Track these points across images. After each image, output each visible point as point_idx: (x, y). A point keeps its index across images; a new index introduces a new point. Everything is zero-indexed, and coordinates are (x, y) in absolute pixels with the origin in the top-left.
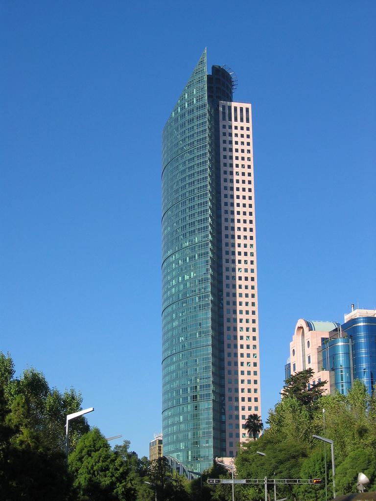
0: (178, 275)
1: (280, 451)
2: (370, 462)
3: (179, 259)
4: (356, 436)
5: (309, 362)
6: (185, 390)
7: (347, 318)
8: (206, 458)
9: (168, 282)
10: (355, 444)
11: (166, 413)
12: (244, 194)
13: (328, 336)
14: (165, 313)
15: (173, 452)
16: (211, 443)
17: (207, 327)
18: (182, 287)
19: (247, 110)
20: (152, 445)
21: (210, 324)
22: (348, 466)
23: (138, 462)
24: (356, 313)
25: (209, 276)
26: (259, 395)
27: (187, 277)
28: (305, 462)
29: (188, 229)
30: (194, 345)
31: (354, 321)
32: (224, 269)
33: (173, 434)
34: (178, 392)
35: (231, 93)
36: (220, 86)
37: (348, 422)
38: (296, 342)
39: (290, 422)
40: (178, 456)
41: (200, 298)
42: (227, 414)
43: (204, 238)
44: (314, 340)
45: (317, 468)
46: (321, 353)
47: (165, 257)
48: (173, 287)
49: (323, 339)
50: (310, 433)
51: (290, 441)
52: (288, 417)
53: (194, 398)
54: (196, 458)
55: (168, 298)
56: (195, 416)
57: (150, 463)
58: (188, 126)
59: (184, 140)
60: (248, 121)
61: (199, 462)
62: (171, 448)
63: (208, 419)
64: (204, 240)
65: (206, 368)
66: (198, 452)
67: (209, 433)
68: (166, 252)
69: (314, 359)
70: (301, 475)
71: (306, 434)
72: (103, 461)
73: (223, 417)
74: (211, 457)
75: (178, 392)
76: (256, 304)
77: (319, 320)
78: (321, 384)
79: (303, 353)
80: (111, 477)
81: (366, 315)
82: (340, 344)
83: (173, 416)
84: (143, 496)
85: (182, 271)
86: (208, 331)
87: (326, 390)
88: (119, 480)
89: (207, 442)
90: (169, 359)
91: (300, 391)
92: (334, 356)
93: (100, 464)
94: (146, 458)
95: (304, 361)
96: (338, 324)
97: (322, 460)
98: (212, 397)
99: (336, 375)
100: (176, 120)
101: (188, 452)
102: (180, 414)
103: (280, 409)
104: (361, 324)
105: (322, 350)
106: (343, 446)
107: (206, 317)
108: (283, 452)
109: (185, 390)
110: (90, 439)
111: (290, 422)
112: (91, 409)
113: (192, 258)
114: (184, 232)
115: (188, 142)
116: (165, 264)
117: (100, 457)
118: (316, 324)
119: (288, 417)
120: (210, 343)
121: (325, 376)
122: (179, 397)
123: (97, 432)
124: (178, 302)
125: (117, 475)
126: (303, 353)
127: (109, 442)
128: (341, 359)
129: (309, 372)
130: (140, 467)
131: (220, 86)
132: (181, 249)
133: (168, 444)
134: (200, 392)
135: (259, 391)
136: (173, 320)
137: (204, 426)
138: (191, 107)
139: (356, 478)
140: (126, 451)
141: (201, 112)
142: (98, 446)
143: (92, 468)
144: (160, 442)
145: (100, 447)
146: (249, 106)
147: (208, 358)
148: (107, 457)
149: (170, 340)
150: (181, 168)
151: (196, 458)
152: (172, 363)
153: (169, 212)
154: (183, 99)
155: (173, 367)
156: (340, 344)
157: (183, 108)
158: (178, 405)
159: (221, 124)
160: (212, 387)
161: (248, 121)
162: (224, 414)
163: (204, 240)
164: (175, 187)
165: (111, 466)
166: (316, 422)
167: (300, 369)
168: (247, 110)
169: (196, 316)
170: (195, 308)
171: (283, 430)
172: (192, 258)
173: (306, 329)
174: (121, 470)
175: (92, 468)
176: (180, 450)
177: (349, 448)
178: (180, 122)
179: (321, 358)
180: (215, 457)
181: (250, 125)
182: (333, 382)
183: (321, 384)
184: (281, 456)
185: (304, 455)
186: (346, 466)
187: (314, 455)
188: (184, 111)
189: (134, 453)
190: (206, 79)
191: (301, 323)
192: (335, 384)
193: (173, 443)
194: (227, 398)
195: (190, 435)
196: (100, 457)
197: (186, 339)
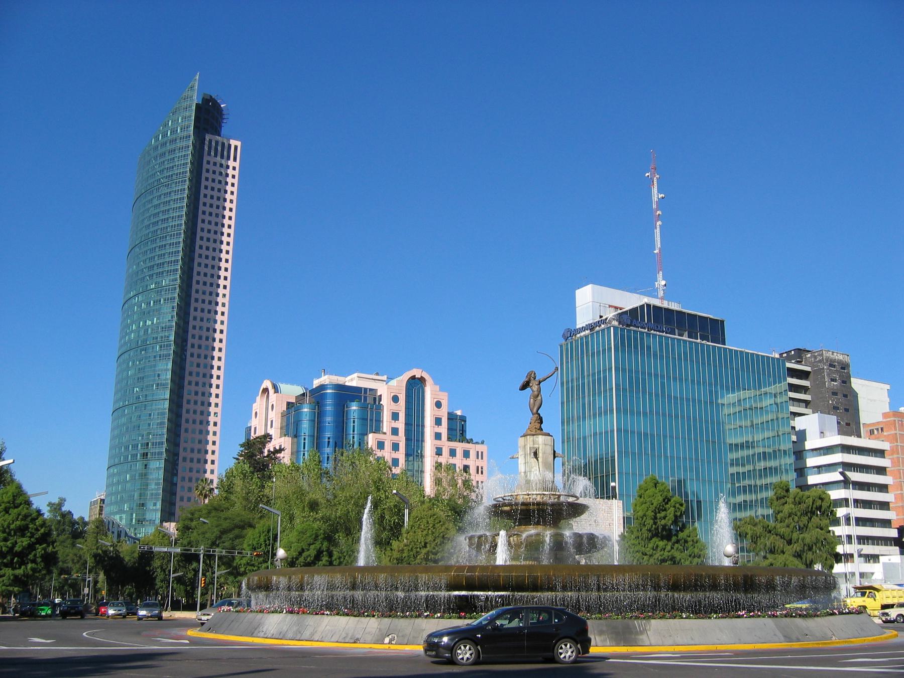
0: (140, 319)
1: (226, 519)
2: (317, 536)
3: (142, 301)
4: (306, 509)
5: (272, 426)
6: (135, 446)
7: (316, 383)
8: (152, 522)
9: (128, 326)
10: (304, 517)
11: (111, 470)
12: (210, 227)
13: (294, 401)
14: (121, 360)
15: (117, 513)
16: (159, 506)
17: (166, 379)
18: (142, 333)
19: (236, 147)
20: (93, 504)
21: (169, 376)
22: (294, 540)
23: (73, 523)
24: (325, 379)
25: (174, 324)
26: (220, 460)
27: (149, 323)
28: (249, 532)
29: (156, 270)
30: (149, 398)
31: (322, 387)
32: (191, 318)
33: (117, 493)
34: (127, 448)
35: (221, 127)
36: (209, 117)
37: (300, 493)
38: (259, 405)
39: (239, 489)
40: (121, 518)
41: (161, 347)
42: (180, 475)
43: (172, 281)
44: (278, 403)
45: (262, 540)
46: (285, 418)
47: (127, 297)
48: (132, 331)
49: (288, 404)
50: (257, 503)
51: (238, 509)
52: (238, 483)
53: (145, 455)
54: (140, 521)
55: (125, 343)
56: (144, 476)
57: (86, 524)
58: (168, 157)
59: (162, 171)
60: (235, 160)
61: (143, 526)
62: (114, 508)
63: (159, 479)
64: (172, 283)
65: (162, 423)
66: (144, 514)
67: (157, 494)
68: (129, 292)
69: (277, 424)
70: (245, 546)
71: (257, 503)
72: (22, 520)
73: (175, 479)
74: (158, 521)
75: (127, 448)
76: (223, 359)
77: (287, 383)
78: (281, 450)
79: (266, 417)
80: (31, 537)
81: (335, 382)
82: (306, 409)
83: (119, 474)
84: (73, 560)
85: (145, 315)
86: (167, 384)
87: (286, 458)
88: (40, 541)
89: (155, 504)
90: (120, 411)
91: (255, 456)
92: (297, 423)
93: (18, 523)
94: (83, 518)
95: (266, 425)
96: (306, 389)
97: (268, 532)
98: (164, 455)
99: (298, 444)
100: (156, 148)
101: (132, 515)
102: (127, 472)
103: (230, 475)
104: (329, 391)
105: (285, 415)
106: (292, 518)
107: (166, 369)
108: (228, 521)
109: (135, 446)
110: (10, 494)
111: (239, 489)
112: (11, 461)
113: (157, 302)
114: (151, 273)
115: (166, 174)
116: (126, 306)
117: (19, 515)
118: (283, 387)
119: (238, 483)
120: (168, 396)
121: (286, 442)
122: (127, 454)
123: (19, 487)
124: (136, 349)
125: (37, 536)
126: (266, 417)
127: (31, 499)
128: (305, 426)
129: (267, 437)
130: (75, 530)
131: (209, 117)
132: (146, 290)
133: (111, 504)
134: (151, 449)
135: (217, 453)
136: (128, 368)
137: (153, 486)
138: (174, 136)
139: (113, 616)
140: (60, 509)
141: (184, 144)
142: (18, 501)
143: (8, 527)
144: (103, 501)
145: (21, 504)
146: (239, 144)
147: (164, 414)
148: (26, 517)
149: (123, 389)
150: (156, 202)
151: (140, 521)
152: (123, 415)
153: (137, 250)
154: (166, 125)
155: (124, 420)
156: (306, 409)
157: (165, 135)
158: (126, 461)
159: (206, 158)
160: (165, 445)
161: (235, 160)
162: (176, 475)
163: (172, 283)
164: (146, 223)
165: (31, 526)
166: (267, 491)
167: (260, 432)
168: (236, 147)
169: (155, 366)
170: (155, 357)
171: (233, 497)
172: (157, 302)
173: (271, 391)
174: (42, 530)
175: (8, 527)
176: (124, 512)
177: (298, 521)
178: (160, 151)
179: (285, 424)
180: (161, 522)
181: (237, 164)
182: (295, 450)
183: (281, 450)
184: (226, 525)
185: (251, 526)
186: (291, 539)
187: (261, 526)
188: (165, 139)
189: (70, 512)
190: (194, 108)
191: (267, 384)
192: (295, 453)
193: (116, 503)
194: (181, 458)
195: (136, 496)
196: (19, 515)
197: (142, 390)
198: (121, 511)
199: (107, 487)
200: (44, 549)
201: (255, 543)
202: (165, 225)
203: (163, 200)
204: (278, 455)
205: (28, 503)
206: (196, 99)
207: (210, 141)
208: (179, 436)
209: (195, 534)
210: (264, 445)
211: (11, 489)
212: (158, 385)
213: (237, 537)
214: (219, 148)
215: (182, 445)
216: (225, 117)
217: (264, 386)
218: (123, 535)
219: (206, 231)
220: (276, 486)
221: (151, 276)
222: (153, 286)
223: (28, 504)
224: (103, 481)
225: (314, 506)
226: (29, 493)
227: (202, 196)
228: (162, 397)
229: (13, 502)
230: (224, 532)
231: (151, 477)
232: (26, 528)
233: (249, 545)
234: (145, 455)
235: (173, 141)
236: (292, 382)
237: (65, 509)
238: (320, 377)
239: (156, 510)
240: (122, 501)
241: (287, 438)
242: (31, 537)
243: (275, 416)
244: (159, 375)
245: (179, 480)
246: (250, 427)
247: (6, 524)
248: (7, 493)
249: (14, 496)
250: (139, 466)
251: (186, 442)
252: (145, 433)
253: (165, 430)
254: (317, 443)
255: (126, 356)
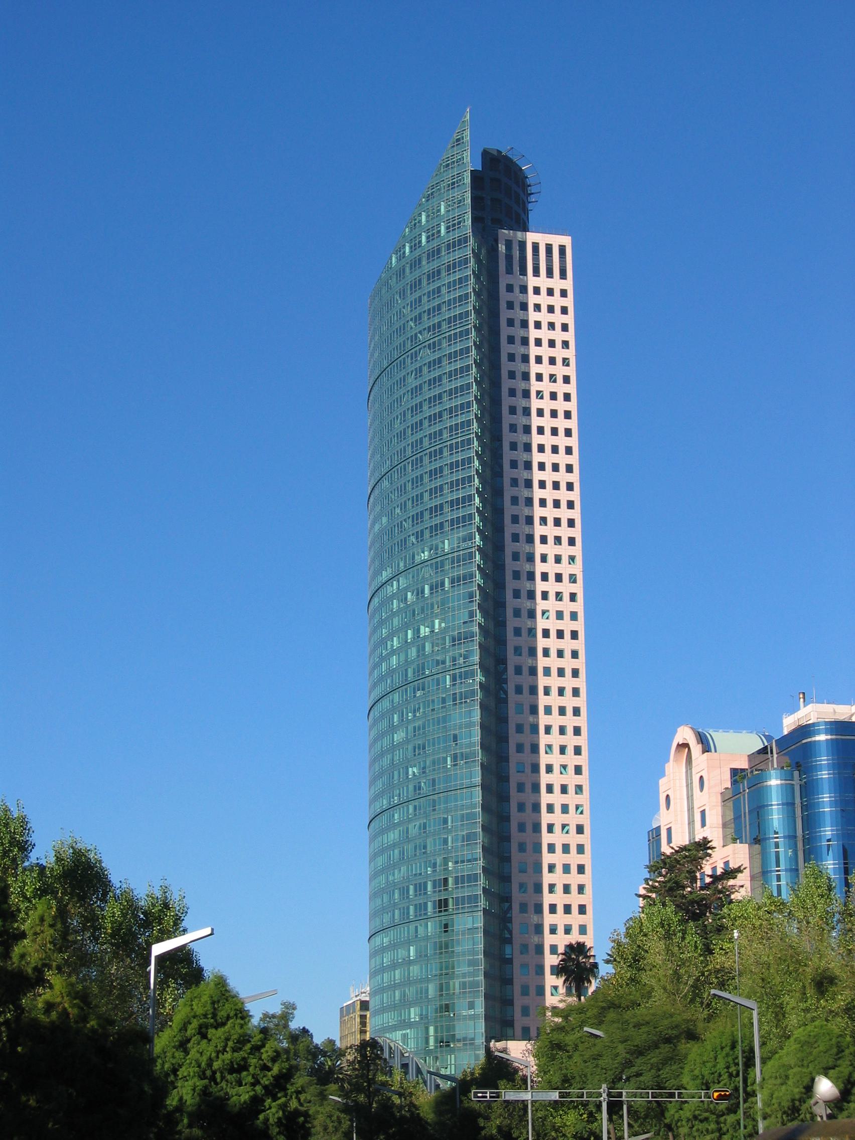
0: (405, 627)
1: (638, 1026)
2: (840, 1051)
3: (406, 589)
4: (810, 992)
5: (703, 824)
6: (421, 888)
7: (789, 723)
8: (469, 1042)
9: (383, 642)
10: (806, 1010)
11: (377, 940)
14: (376, 712)
15: (394, 1028)
17: (471, 745)
18: (413, 652)
19: (562, 249)
20: (345, 1012)
21: (477, 737)
23: (315, 1052)
24: (811, 713)
27: (424, 631)
28: (693, 1051)
30: (440, 786)
31: (804, 731)
32: (509, 612)
33: (393, 987)
34: (404, 892)
35: (526, 211)
36: (501, 196)
37: (792, 961)
39: (659, 960)
40: (405, 1037)
41: (454, 678)
43: (463, 541)
44: (715, 772)
45: (721, 1065)
46: (730, 804)
49: (734, 772)
52: (656, 948)
53: (442, 905)
54: (445, 1043)
55: (382, 678)
56: (445, 948)
58: (427, 287)
59: (418, 319)
60: (563, 275)
61: (452, 1051)
62: (389, 1018)
64: (463, 545)
65: (470, 837)
66: (450, 1028)
67: (474, 984)
69: (715, 817)
70: (686, 1079)
71: (697, 988)
72: (234, 1050)
73: (508, 949)
74: (481, 1040)
75: (404, 892)
78: (730, 873)
79: (690, 803)
80: (253, 1085)
81: (831, 718)
82: (774, 782)
83: (393, 946)
84: (325, 1128)
86: (474, 754)
87: (743, 888)
89: (471, 1006)
90: (384, 817)
91: (683, 888)
92: (759, 811)
93: (228, 1056)
94: (331, 1042)
95: (691, 822)
96: (769, 738)
97: (733, 1047)
98: (482, 903)
99: (764, 854)
100: (401, 273)
102: (408, 943)
103: (636, 930)
104: (822, 737)
105: (732, 797)
106: (780, 1013)
107: (469, 722)
108: (644, 1029)
109: (421, 888)
110: (205, 998)
111: (659, 960)
112: (208, 931)
115: (427, 322)
116: (376, 600)
117: (227, 1039)
118: (719, 737)
119: (656, 948)
120: (478, 779)
121: (738, 854)
122: (406, 904)
123: (221, 982)
124: (405, 686)
126: (690, 803)
127: (248, 1006)
131: (501, 196)
132: (412, 566)
133: (383, 1010)
134: (454, 892)
135: (588, 890)
136: (392, 729)
137: (465, 969)
138: (435, 244)
140: (286, 1026)
141: (457, 255)
142: (222, 1014)
144: (364, 1005)
145: (228, 1018)
146: (566, 241)
148: (243, 1040)
149: (386, 775)
150: (412, 382)
151: (445, 1043)
152: (392, 826)
153: (385, 483)
155: (393, 836)
156: (774, 782)
160: (482, 882)
161: (563, 275)
162: (510, 941)
165: (253, 1061)
166: (718, 960)
167: (681, 839)
168: (562, 249)
169: (445, 719)
170: (444, 700)
171: (644, 978)
172: (437, 587)
173: (696, 749)
174: (276, 1070)
176: (408, 1025)
177: (793, 1020)
178: (410, 277)
179: (730, 816)
180: (488, 1041)
182: (758, 870)
183: (730, 873)
184: (640, 1037)
185: (692, 1036)
186: (786, 1060)
187: (714, 1034)
188: (418, 252)
189: (305, 1031)
190: (468, 180)
191: (685, 734)
192: (762, 875)
193: (393, 1007)
194: (516, 907)
196: (227, 1039)
197: (423, 770)
198: (405, 1024)
199: (373, 974)
200: (283, 1107)
201: (706, 1072)
202: (437, 428)
203: (427, 376)
204: (731, 882)
205: (243, 1015)
206: (470, 161)
207: (536, 247)
208: (508, 859)
209: (576, 1058)
210: (696, 862)
211: (206, 991)
212: (455, 758)
213: (666, 1061)
214: (516, 254)
215: (517, 878)
216: (533, 189)
217: (678, 739)
218: (412, 1070)
219: (561, 432)
220: (738, 947)
221: (419, 535)
222: (425, 555)
223: (243, 1018)
224: (363, 965)
225: (824, 983)
226: (242, 995)
227: (504, 358)
228: (466, 782)
229: (214, 1016)
230: (639, 1052)
231: (458, 949)
232: (243, 1067)
233: (695, 1078)
234: (442, 905)
235: (434, 254)
236: (737, 726)
237: (295, 1025)
238: (795, 709)
239: (474, 1017)
240: (405, 1003)
241: (738, 845)
242: (253, 1085)
243: (711, 802)
244: (455, 738)
245: (517, 952)
246: (658, 828)
247: (204, 1060)
248: (199, 997)
249: (213, 1003)
250: (431, 927)
251: (523, 871)
252: (439, 861)
253: (479, 850)
254: (807, 846)
255: (386, 704)
